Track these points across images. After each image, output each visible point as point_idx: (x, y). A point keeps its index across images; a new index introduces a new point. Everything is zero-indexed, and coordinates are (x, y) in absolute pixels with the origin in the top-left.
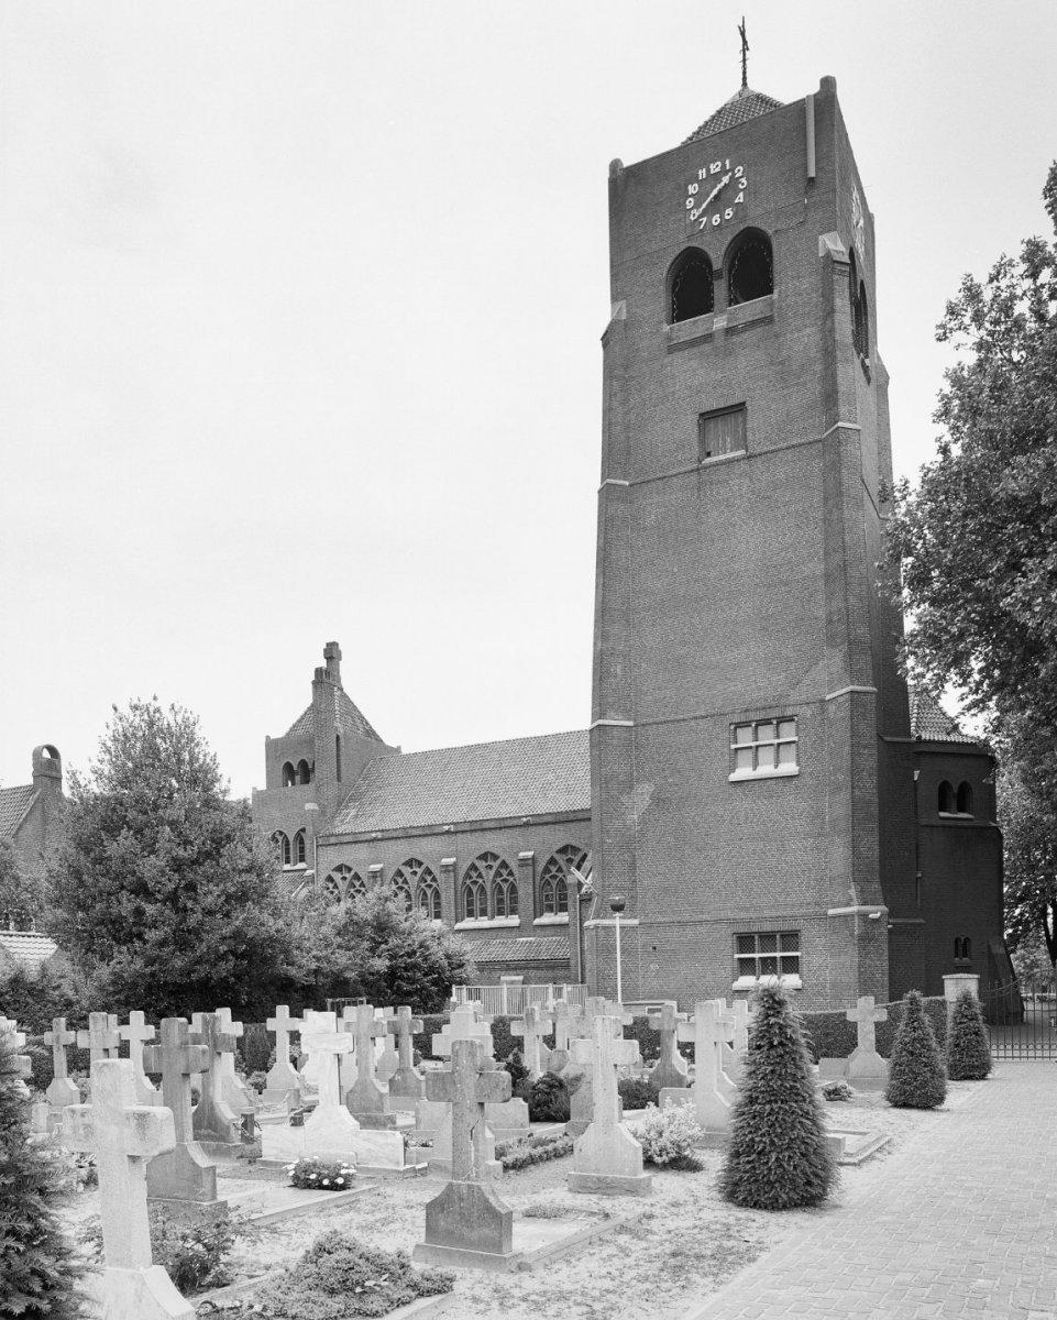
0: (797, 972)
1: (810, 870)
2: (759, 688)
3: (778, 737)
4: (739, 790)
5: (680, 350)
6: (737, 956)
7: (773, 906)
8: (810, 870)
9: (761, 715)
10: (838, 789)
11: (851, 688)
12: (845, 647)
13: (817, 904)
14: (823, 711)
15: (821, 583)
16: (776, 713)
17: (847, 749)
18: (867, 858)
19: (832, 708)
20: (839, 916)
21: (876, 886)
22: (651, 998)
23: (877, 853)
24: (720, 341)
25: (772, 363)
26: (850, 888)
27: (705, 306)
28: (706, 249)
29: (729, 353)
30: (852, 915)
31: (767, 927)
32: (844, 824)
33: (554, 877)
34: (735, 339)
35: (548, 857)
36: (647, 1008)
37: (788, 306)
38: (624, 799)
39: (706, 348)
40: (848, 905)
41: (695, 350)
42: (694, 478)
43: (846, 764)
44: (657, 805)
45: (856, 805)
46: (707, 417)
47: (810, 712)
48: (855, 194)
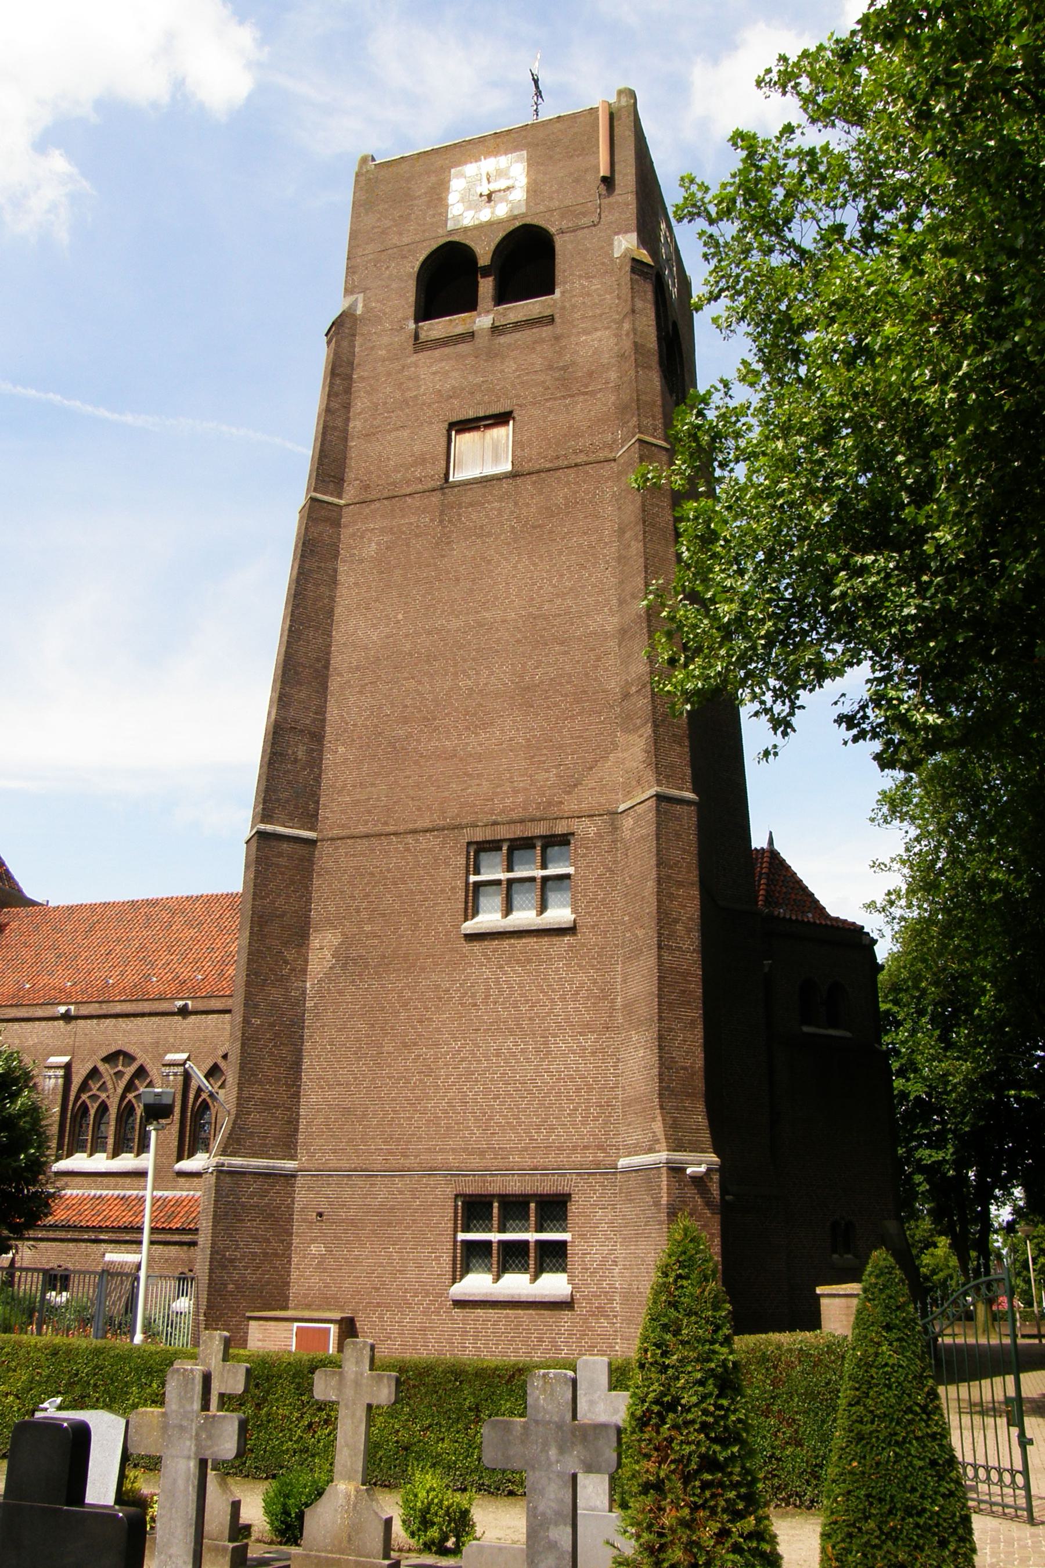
0: (564, 1270)
1: (590, 1089)
2: (516, 791)
3: (510, 869)
4: (477, 946)
5: (430, 348)
6: (462, 1236)
7: (525, 1149)
8: (590, 1089)
9: (518, 831)
10: (634, 955)
11: (659, 789)
12: (648, 730)
13: (601, 1148)
14: (615, 828)
15: (612, 644)
16: (540, 829)
17: (651, 885)
18: (685, 1069)
19: (628, 822)
20: (637, 1170)
21: (701, 1119)
22: (308, 1307)
23: (700, 1063)
24: (481, 341)
25: (550, 368)
26: (654, 1119)
27: (470, 304)
28: (472, 244)
29: (493, 355)
30: (655, 1168)
31: (514, 1186)
32: (647, 1009)
33: (94, 1097)
34: (503, 340)
35: (89, 1066)
36: (296, 1324)
37: (574, 306)
38: (290, 955)
39: (463, 348)
40: (651, 1150)
41: (447, 350)
42: (435, 499)
43: (650, 907)
44: (344, 967)
45: (665, 978)
46: (452, 426)
47: (592, 830)
48: (663, 226)
